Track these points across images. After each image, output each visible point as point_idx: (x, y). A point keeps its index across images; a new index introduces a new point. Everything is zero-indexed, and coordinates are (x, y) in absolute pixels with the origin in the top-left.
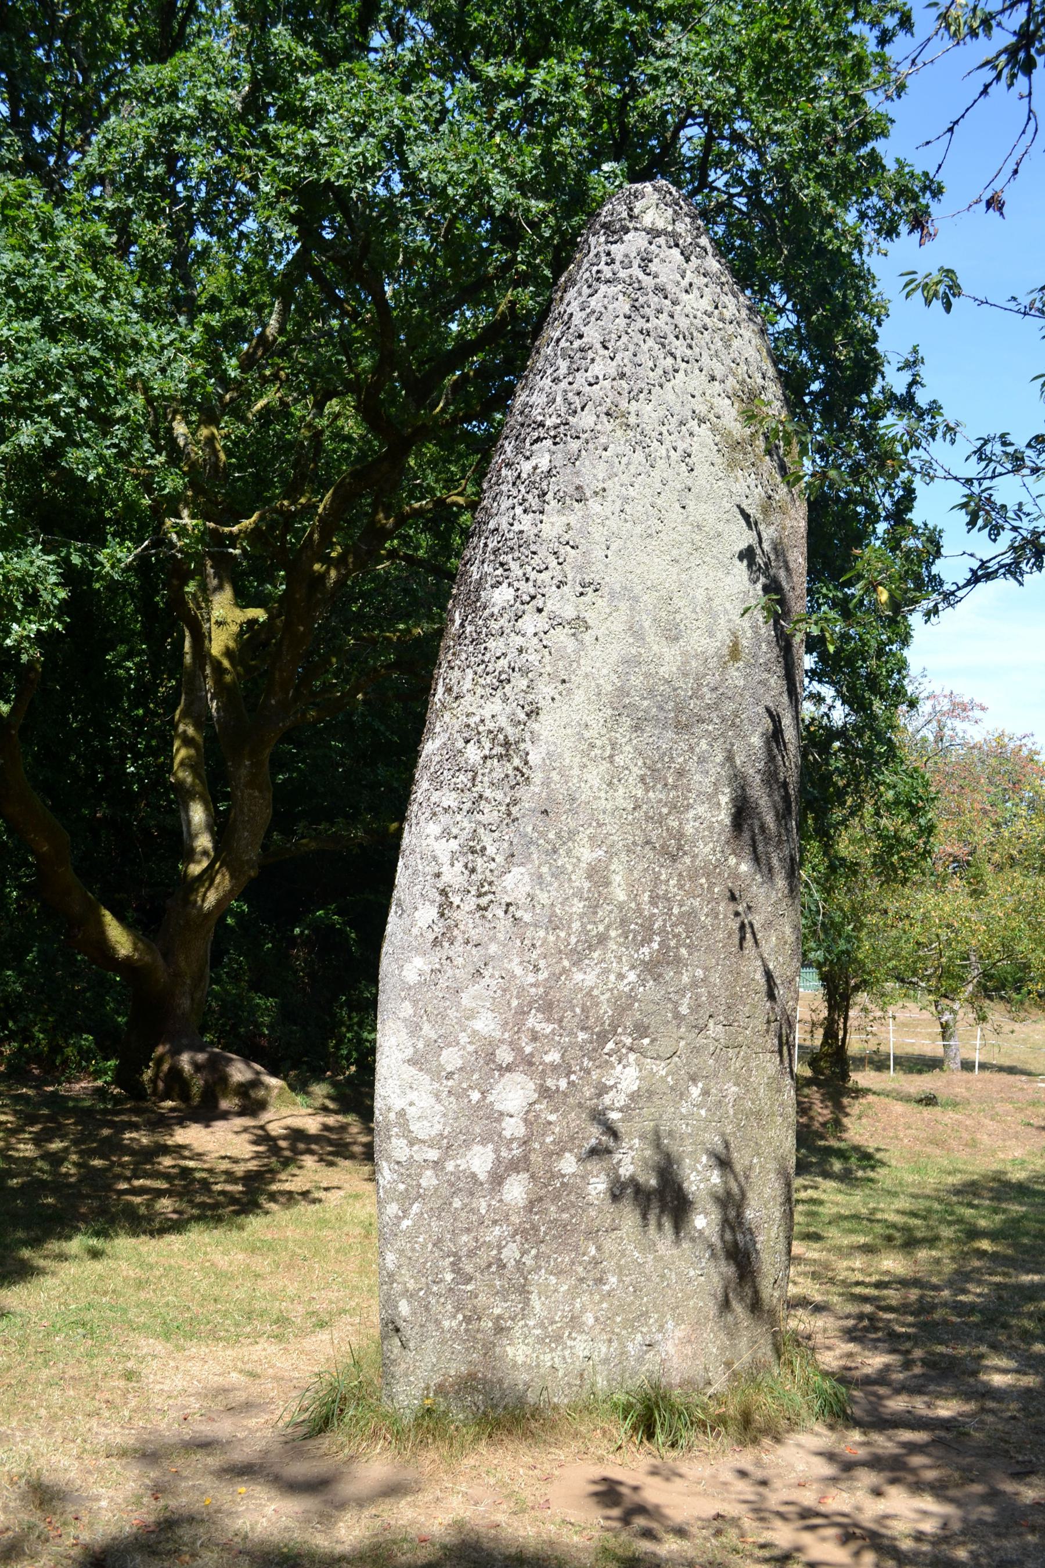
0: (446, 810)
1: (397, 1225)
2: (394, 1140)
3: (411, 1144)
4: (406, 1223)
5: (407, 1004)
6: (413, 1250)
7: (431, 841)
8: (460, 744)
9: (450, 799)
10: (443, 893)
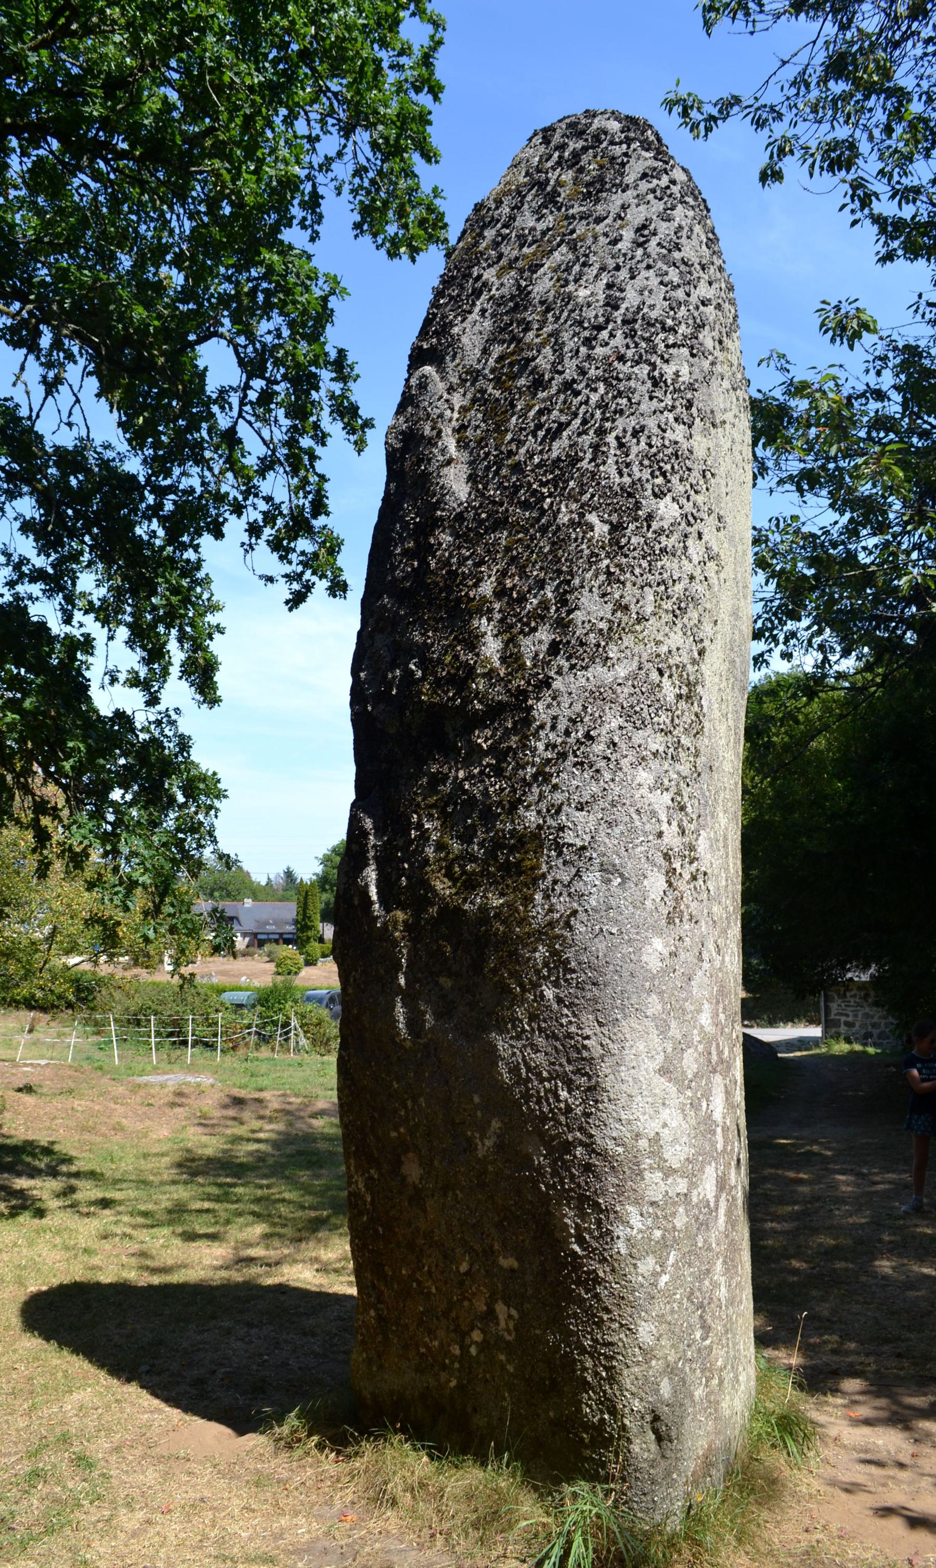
0: (655, 754)
1: (654, 1285)
2: (647, 1175)
3: (666, 1176)
4: (665, 1278)
5: (654, 998)
6: (672, 1311)
7: (644, 791)
8: (655, 676)
9: (657, 743)
10: (667, 857)
